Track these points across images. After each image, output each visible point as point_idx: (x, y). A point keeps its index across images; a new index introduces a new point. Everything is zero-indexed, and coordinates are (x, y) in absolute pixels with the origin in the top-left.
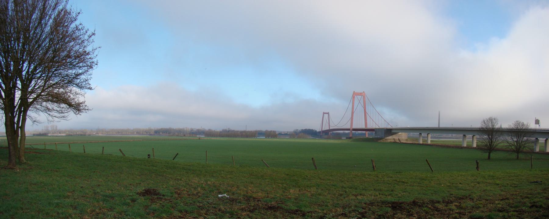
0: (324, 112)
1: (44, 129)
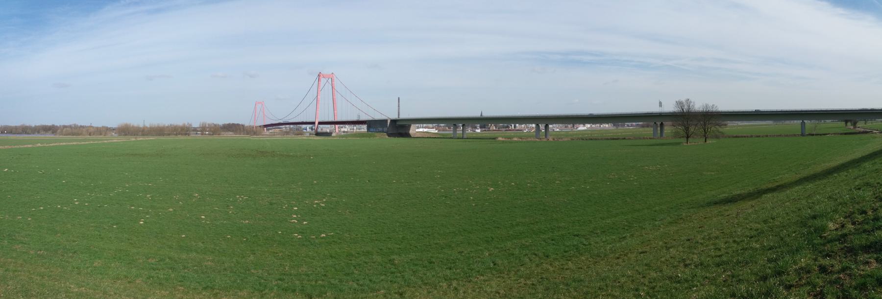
1: (186, 124)
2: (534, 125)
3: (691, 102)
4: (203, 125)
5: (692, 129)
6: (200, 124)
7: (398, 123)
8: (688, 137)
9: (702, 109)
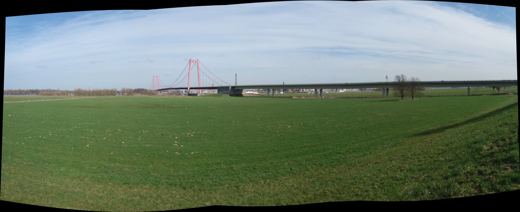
0: (193, 59)
1: (114, 89)
2: (314, 90)
3: (404, 76)
4: (123, 89)
5: (405, 92)
6: (122, 89)
7: (236, 88)
8: (402, 97)
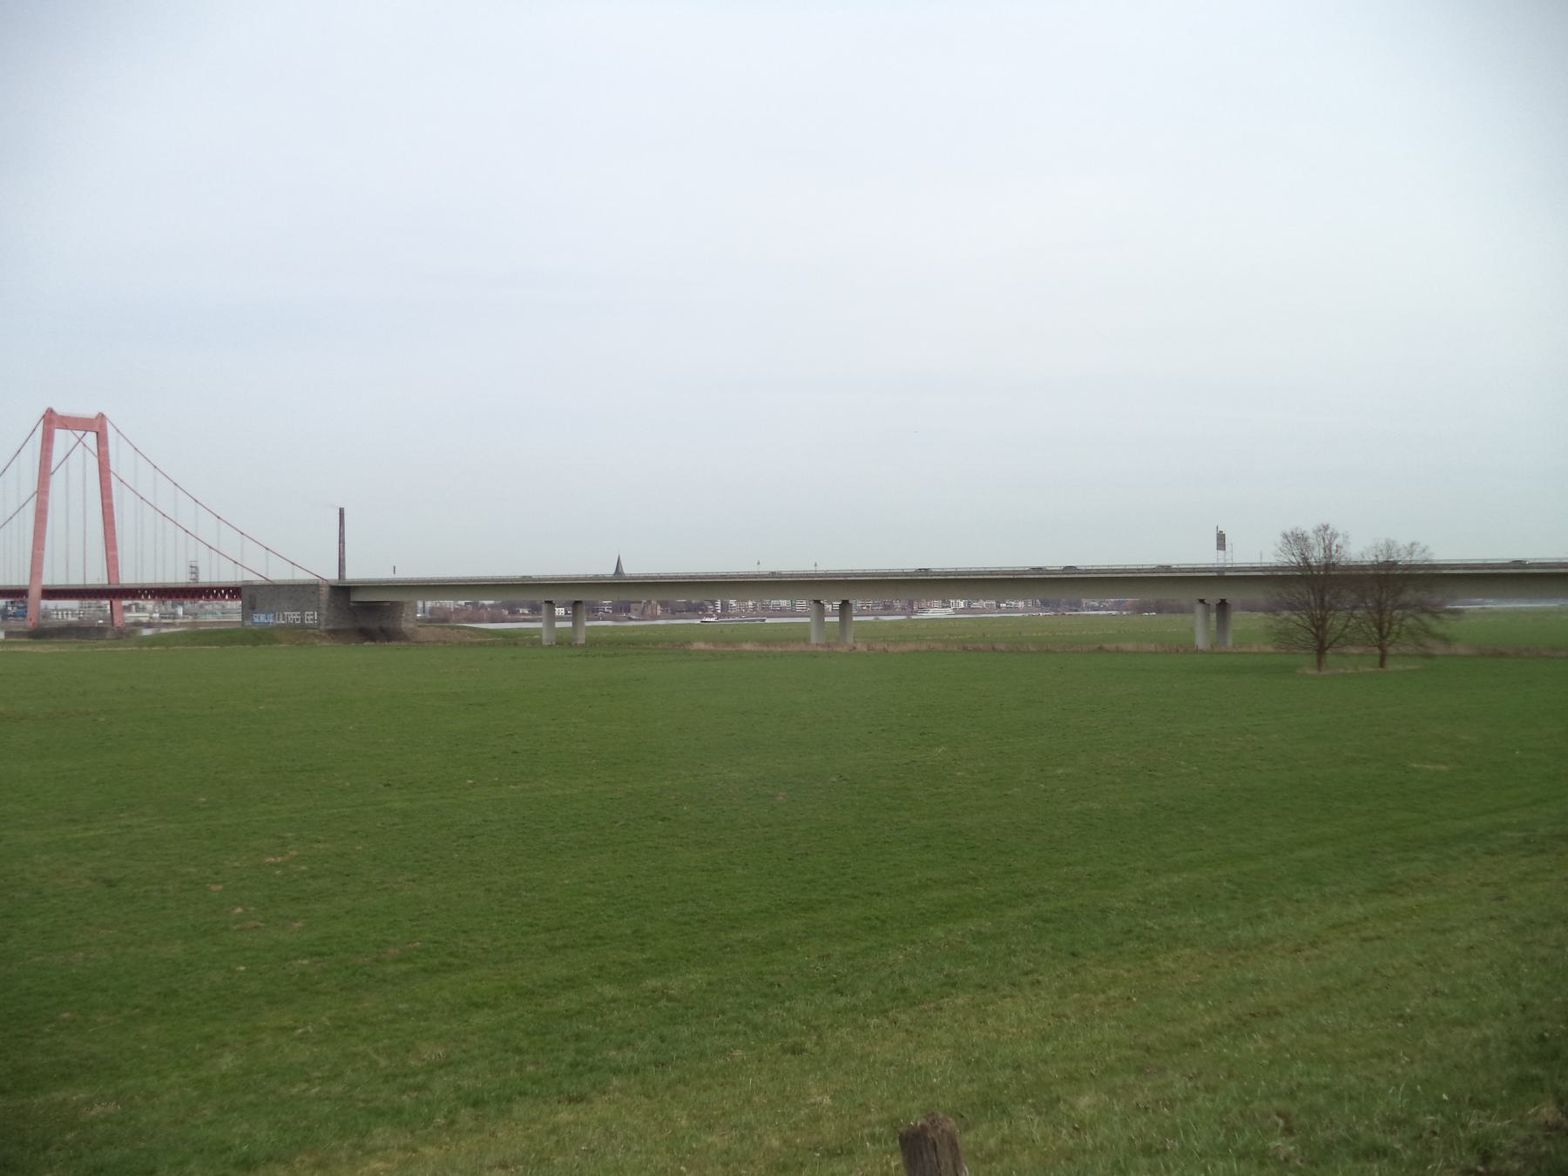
0: (61, 410)
3: (1334, 536)
5: (1336, 622)
8: (1321, 650)
9: (1373, 558)
